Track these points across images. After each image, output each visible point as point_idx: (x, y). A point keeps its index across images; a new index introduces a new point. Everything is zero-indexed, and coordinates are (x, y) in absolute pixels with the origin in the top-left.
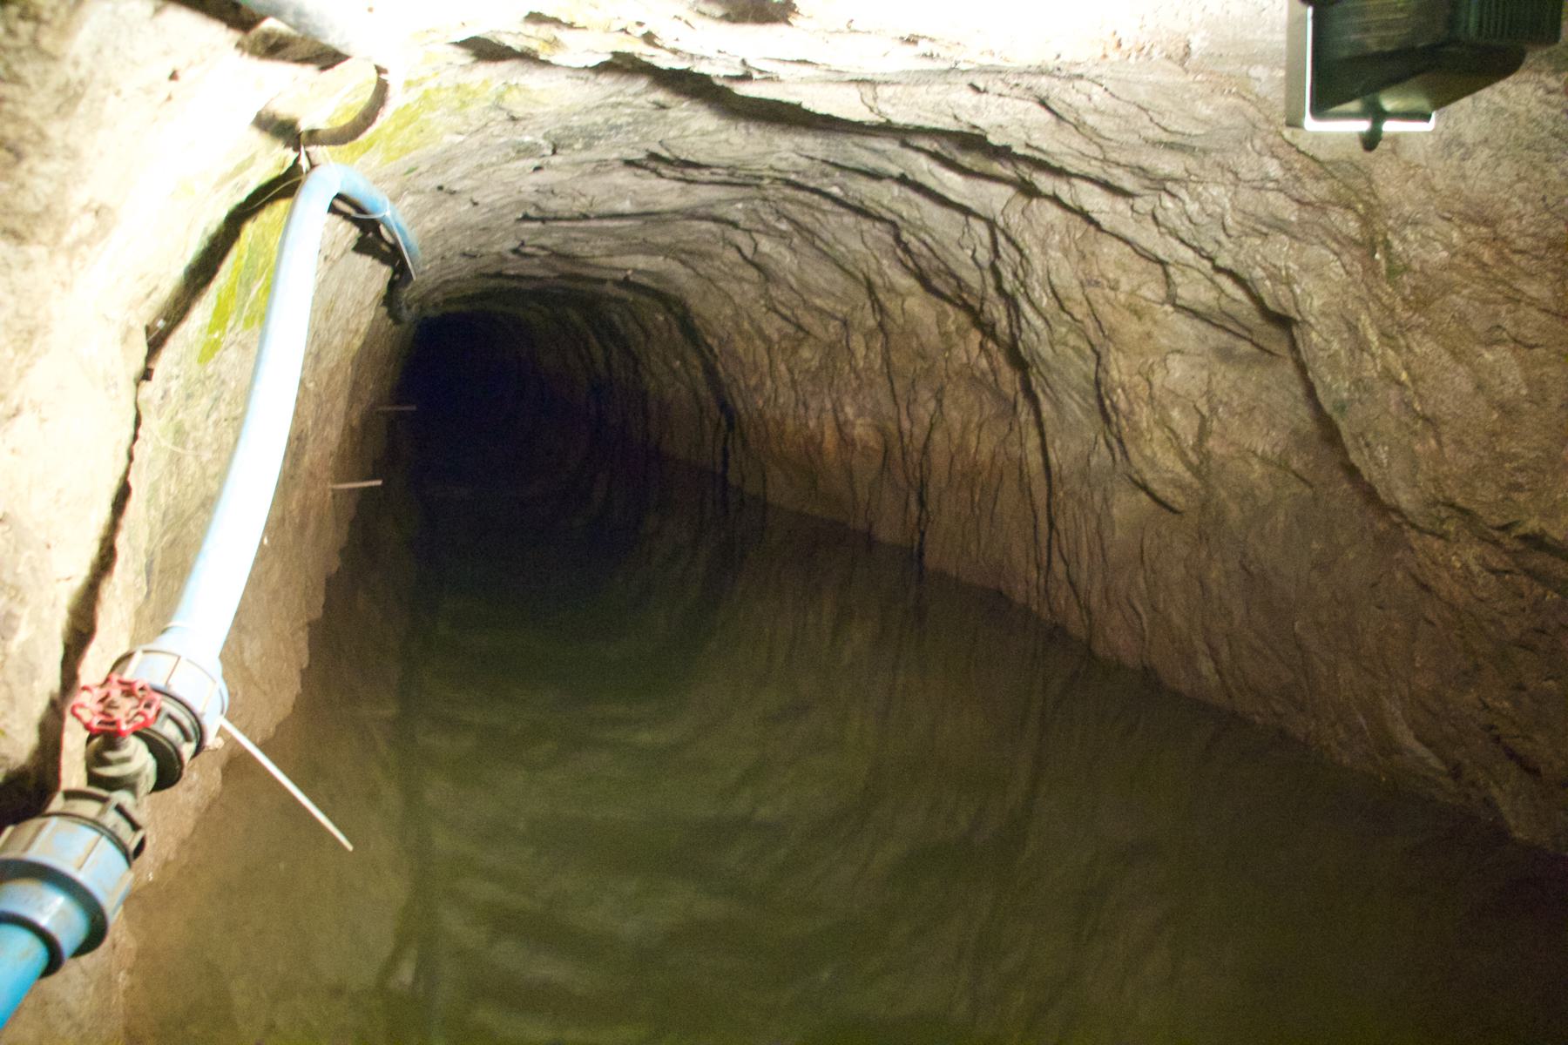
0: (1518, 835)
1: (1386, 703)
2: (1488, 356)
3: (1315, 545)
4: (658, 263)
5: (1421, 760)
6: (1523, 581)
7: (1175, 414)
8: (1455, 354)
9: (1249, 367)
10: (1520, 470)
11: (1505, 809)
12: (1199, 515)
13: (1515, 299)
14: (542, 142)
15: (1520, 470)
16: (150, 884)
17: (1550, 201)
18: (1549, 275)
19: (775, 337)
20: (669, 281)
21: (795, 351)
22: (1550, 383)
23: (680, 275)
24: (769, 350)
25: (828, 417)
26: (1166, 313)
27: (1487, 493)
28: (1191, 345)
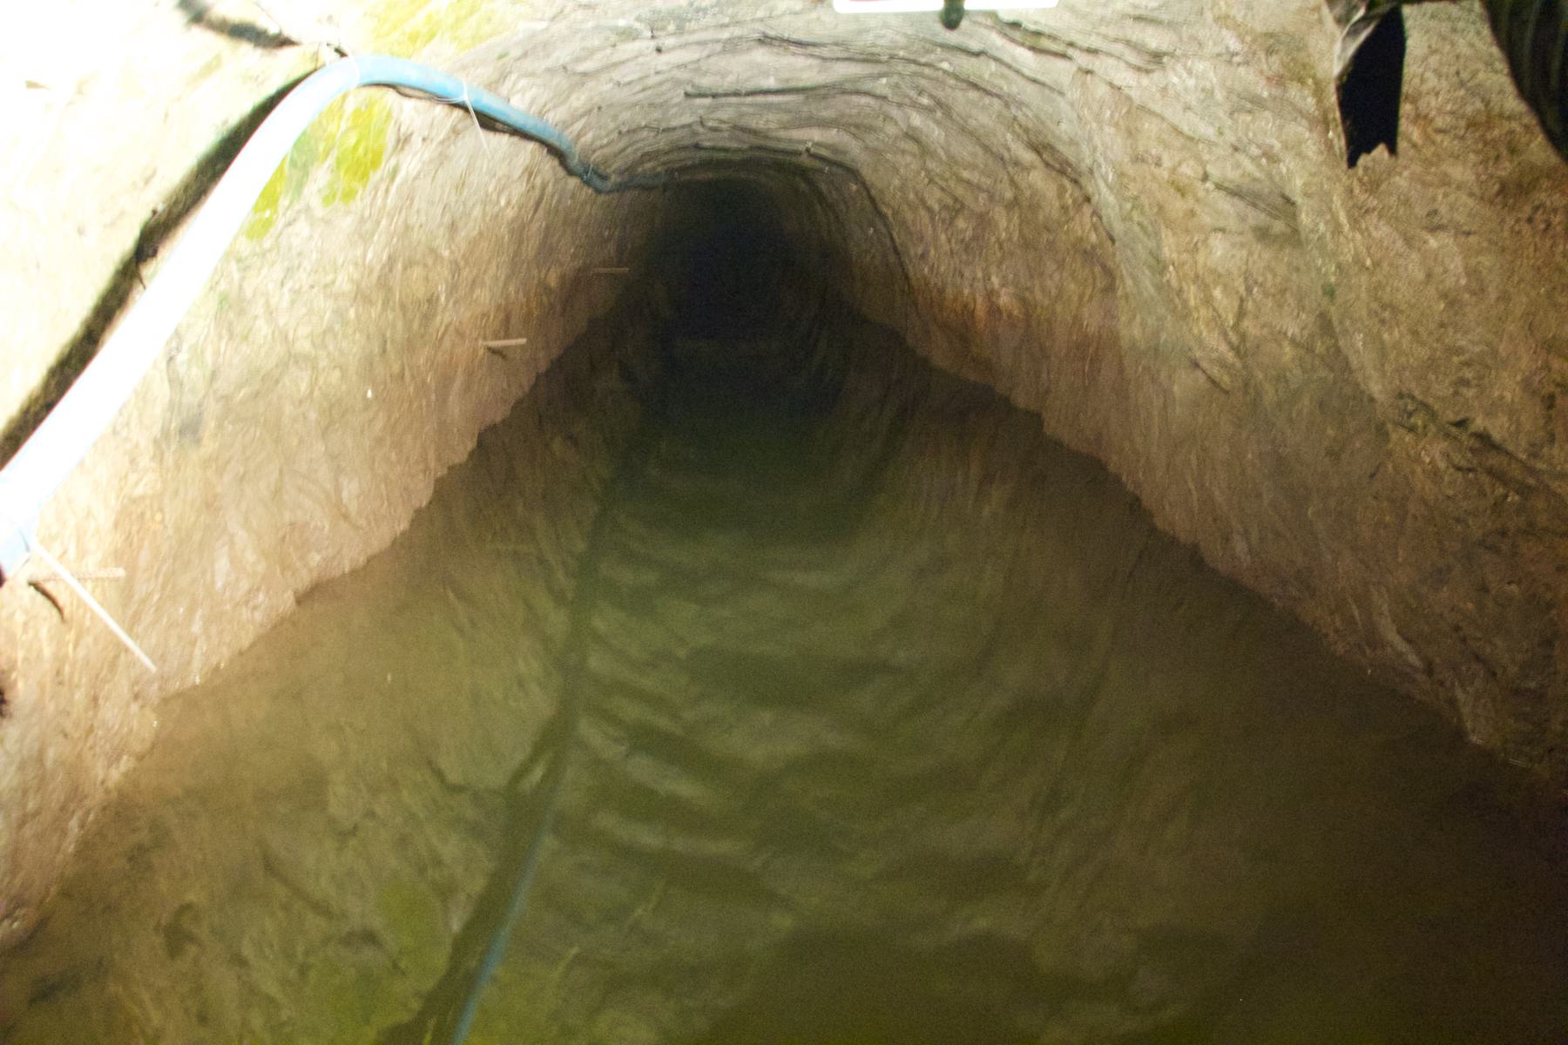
0: (1474, 739)
1: (1375, 597)
2: (1433, 243)
3: (1330, 432)
4: (832, 136)
5: (1400, 655)
6: (1485, 479)
7: (1217, 293)
8: (1408, 241)
9: (1282, 248)
10: (1467, 364)
11: (1466, 710)
12: (1240, 394)
13: (1445, 181)
14: (637, 25)
15: (1467, 364)
16: (195, 687)
17: (1465, 75)
18: (1472, 156)
19: (936, 207)
20: (845, 153)
21: (952, 219)
22: (1485, 272)
23: (854, 149)
24: (932, 219)
25: (979, 285)
26: (1207, 190)
27: (1442, 388)
28: (1232, 223)
